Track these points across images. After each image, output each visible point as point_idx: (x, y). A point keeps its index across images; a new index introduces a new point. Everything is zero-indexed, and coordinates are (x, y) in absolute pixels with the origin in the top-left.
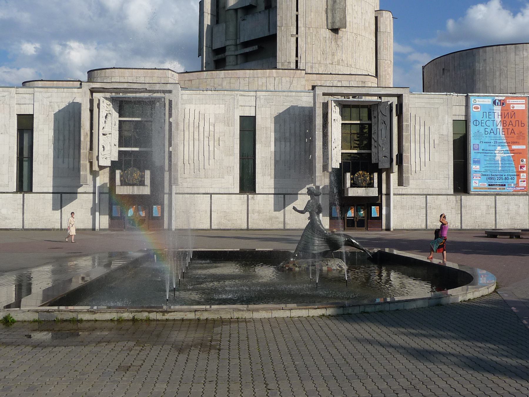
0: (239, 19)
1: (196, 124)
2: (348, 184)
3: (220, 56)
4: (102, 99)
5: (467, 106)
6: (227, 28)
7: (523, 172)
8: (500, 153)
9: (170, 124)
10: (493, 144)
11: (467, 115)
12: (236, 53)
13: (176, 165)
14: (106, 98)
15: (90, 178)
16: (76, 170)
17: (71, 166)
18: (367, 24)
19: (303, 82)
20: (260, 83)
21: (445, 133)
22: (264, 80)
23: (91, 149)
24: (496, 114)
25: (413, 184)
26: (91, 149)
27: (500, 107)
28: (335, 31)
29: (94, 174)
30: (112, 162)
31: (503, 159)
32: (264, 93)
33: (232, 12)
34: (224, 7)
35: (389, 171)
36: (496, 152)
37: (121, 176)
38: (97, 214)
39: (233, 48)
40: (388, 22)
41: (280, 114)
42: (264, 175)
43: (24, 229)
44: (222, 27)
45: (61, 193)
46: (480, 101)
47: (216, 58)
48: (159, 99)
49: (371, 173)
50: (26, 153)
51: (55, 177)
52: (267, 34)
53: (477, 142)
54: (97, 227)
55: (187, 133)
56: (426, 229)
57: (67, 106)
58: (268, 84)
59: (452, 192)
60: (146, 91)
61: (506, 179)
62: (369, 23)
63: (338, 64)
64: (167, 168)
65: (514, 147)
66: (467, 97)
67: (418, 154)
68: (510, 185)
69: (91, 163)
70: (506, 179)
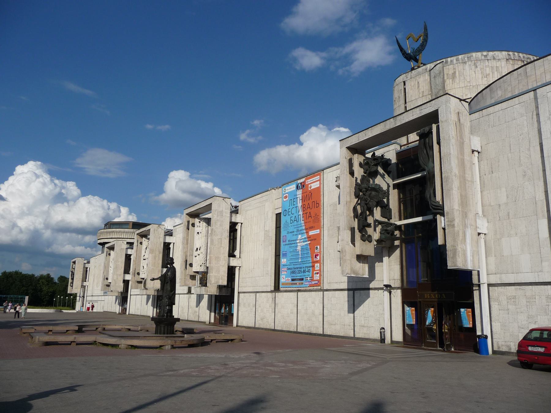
10: (295, 233)
24: (298, 199)
27: (301, 190)
36: (298, 241)
43: (254, 328)
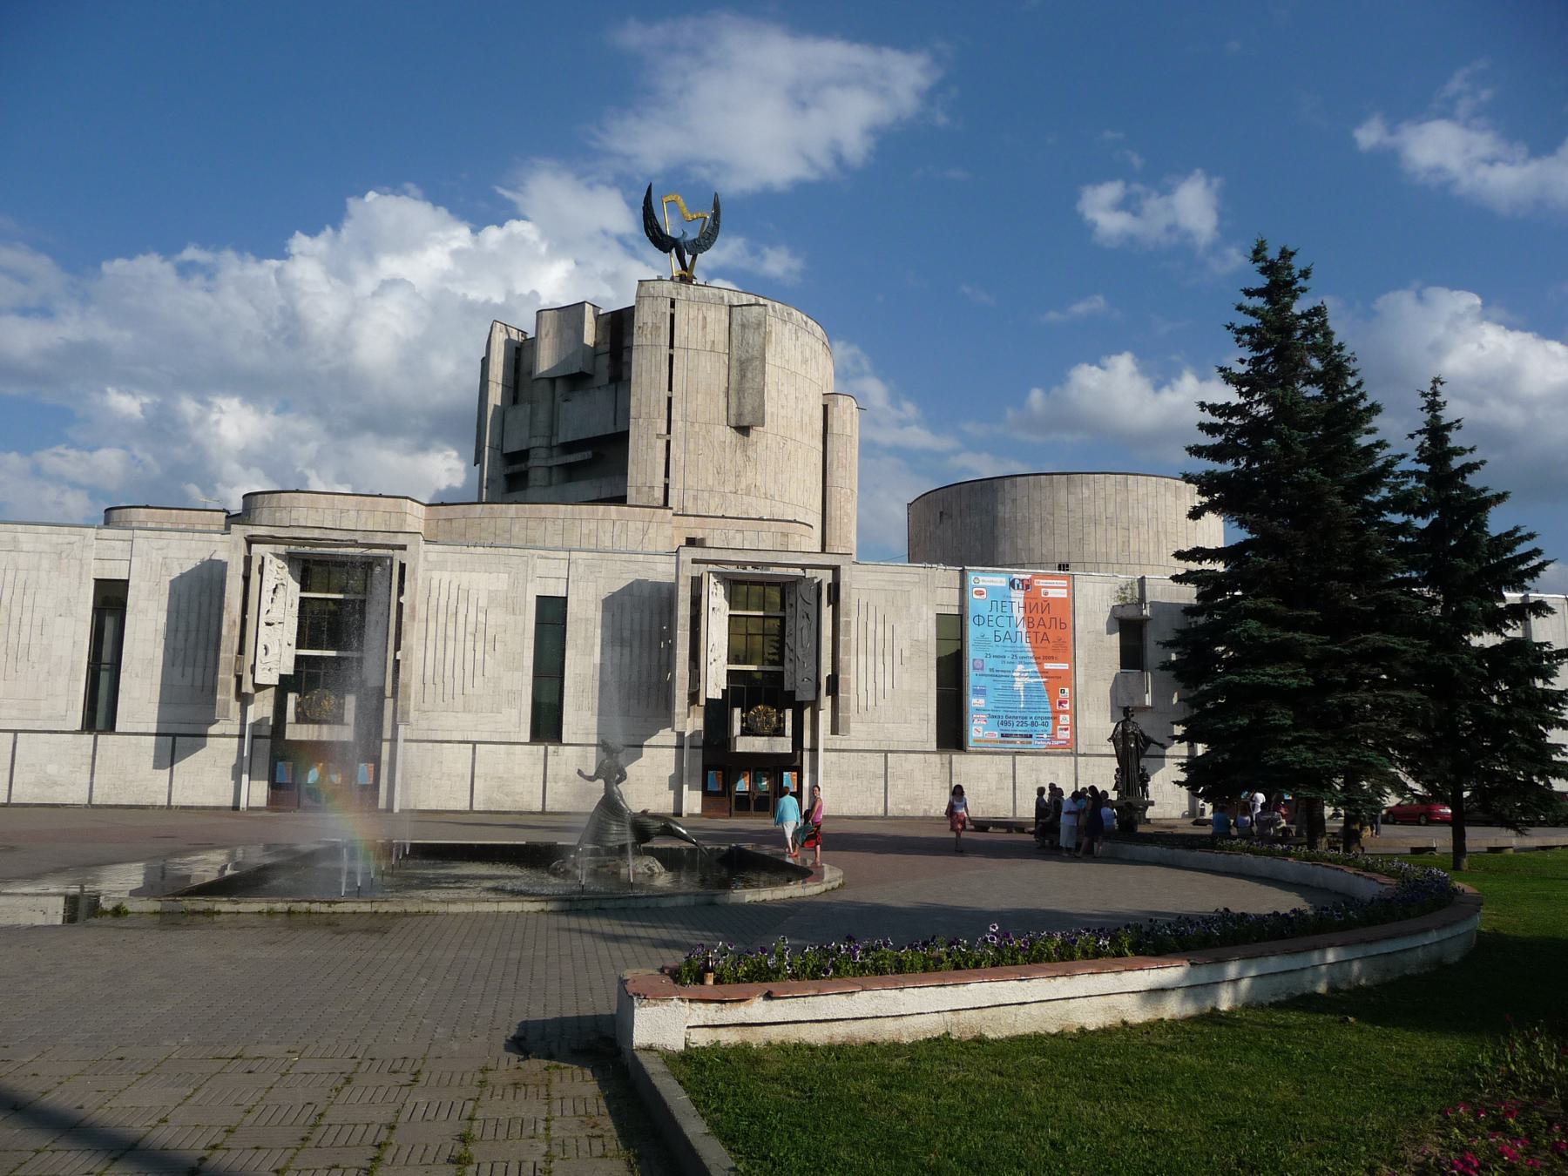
0: (558, 399)
1: (452, 609)
2: (737, 729)
3: (517, 468)
4: (268, 557)
5: (963, 589)
6: (533, 414)
7: (1064, 712)
8: (1023, 676)
9: (400, 605)
11: (963, 605)
12: (551, 463)
13: (407, 686)
14: (277, 556)
15: (235, 706)
16: (209, 690)
17: (198, 683)
18: (806, 419)
19: (668, 530)
20: (585, 531)
21: (922, 637)
22: (593, 525)
23: (241, 651)
24: (1015, 606)
25: (859, 732)
26: (241, 651)
28: (743, 430)
29: (244, 699)
30: (282, 677)
31: (1027, 688)
32: (584, 555)
33: (546, 384)
34: (530, 373)
35: (815, 706)
37: (298, 705)
38: (245, 777)
39: (543, 453)
40: (847, 417)
41: (613, 595)
42: (579, 709)
43: (91, 806)
44: (523, 410)
45: (174, 736)
46: (987, 581)
47: (509, 470)
48: (379, 560)
49: (781, 710)
50: (106, 655)
51: (163, 703)
52: (611, 430)
53: (981, 655)
54: (243, 804)
55: (432, 625)
56: (885, 817)
57: (198, 568)
58: (601, 534)
59: (934, 747)
60: (356, 544)
61: (1033, 724)
62: (811, 417)
63: (748, 494)
64: (388, 692)
65: (1048, 666)
66: (962, 571)
67: (871, 676)
68: (1040, 738)
69: (239, 679)
70: (1033, 724)
